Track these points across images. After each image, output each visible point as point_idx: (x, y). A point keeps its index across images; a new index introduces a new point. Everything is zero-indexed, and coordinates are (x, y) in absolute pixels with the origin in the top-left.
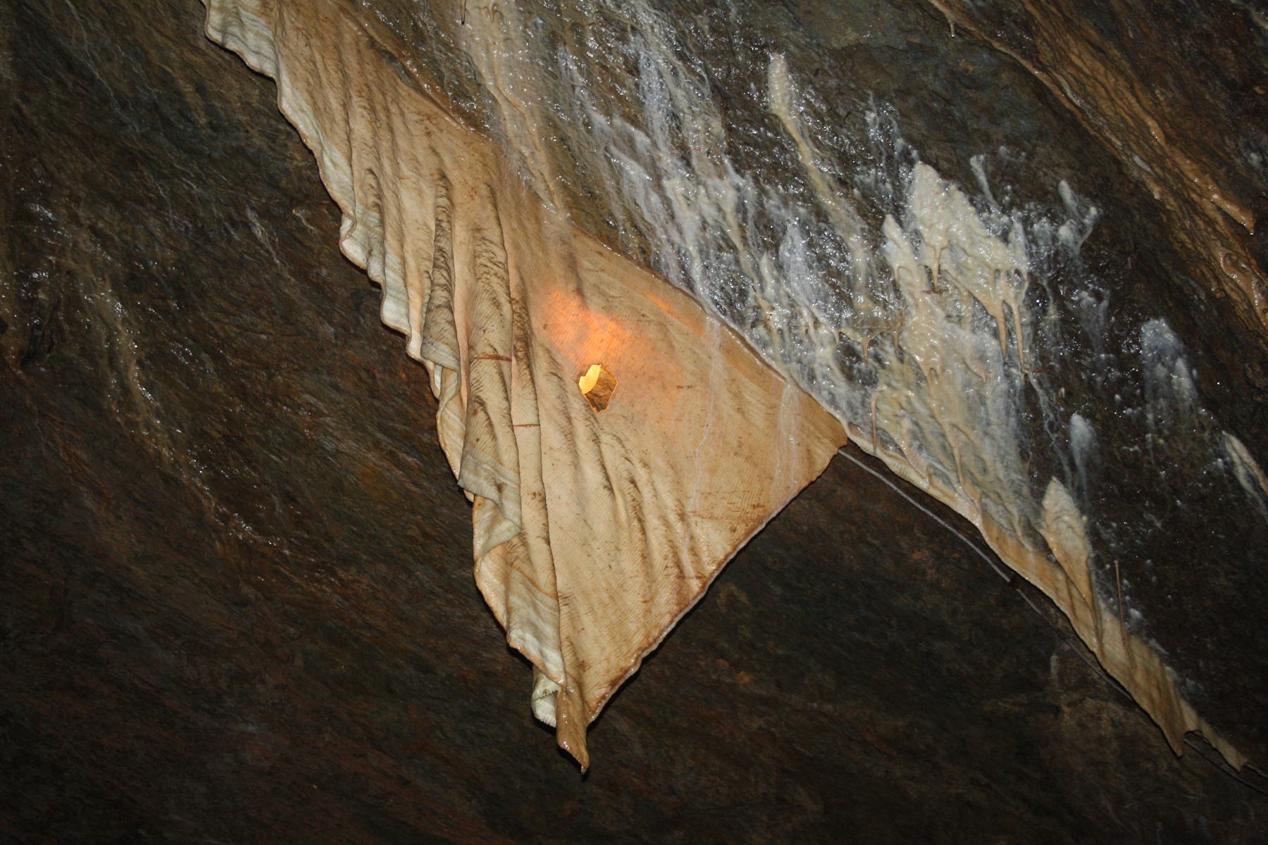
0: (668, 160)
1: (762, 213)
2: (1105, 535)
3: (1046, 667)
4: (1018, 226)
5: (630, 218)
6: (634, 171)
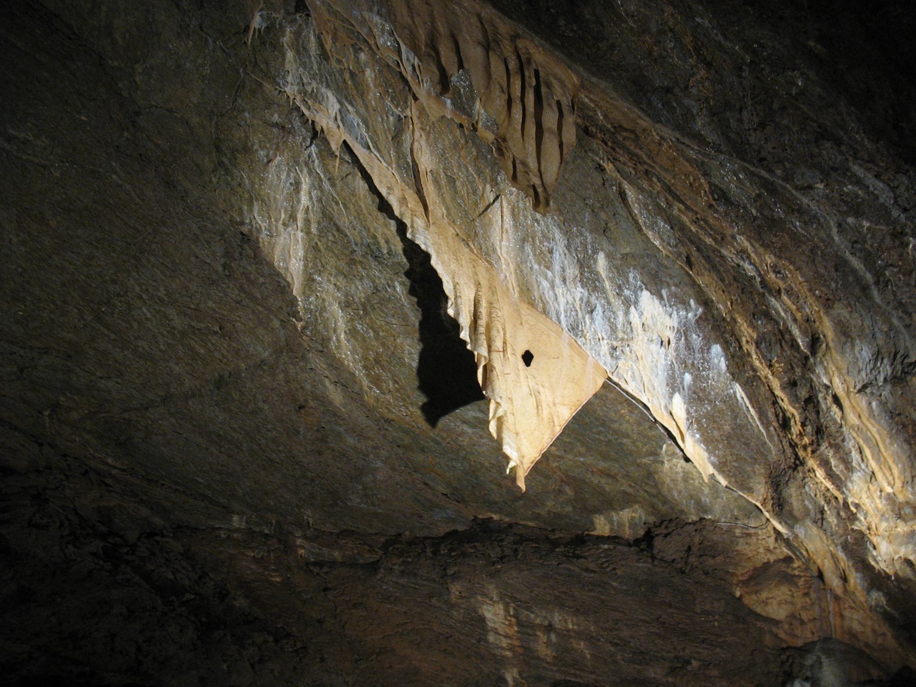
0: (558, 281)
1: (588, 302)
2: (692, 411)
3: (661, 448)
4: (675, 312)
5: (541, 298)
6: (545, 284)
